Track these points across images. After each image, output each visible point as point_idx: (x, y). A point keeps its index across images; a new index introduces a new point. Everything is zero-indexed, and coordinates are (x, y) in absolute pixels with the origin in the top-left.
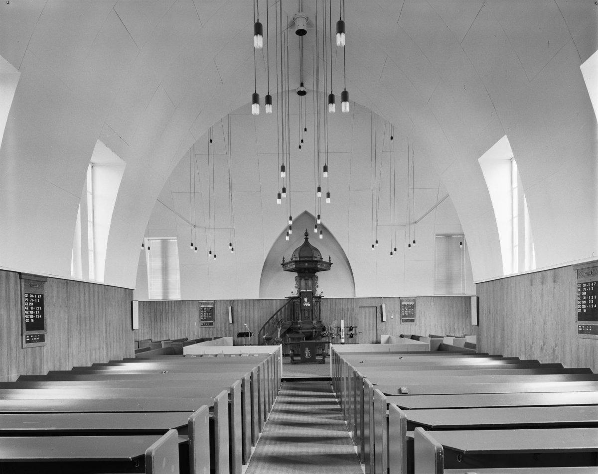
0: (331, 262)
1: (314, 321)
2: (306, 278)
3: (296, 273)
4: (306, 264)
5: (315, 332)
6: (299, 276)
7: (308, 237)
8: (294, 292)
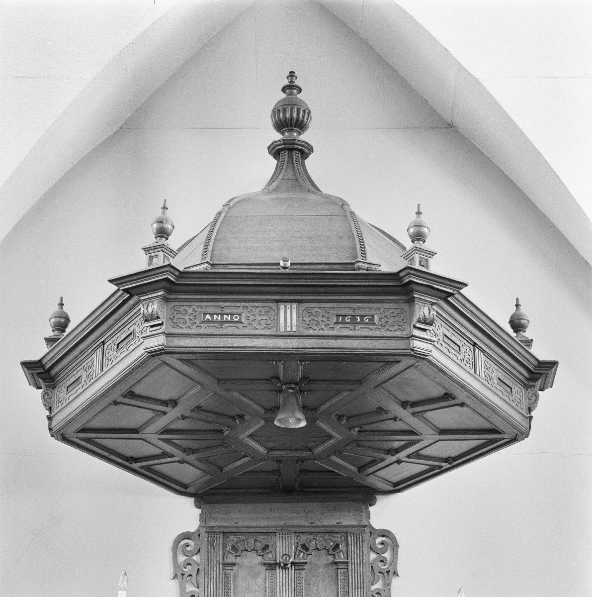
0: (541, 352)
2: (283, 547)
3: (190, 501)
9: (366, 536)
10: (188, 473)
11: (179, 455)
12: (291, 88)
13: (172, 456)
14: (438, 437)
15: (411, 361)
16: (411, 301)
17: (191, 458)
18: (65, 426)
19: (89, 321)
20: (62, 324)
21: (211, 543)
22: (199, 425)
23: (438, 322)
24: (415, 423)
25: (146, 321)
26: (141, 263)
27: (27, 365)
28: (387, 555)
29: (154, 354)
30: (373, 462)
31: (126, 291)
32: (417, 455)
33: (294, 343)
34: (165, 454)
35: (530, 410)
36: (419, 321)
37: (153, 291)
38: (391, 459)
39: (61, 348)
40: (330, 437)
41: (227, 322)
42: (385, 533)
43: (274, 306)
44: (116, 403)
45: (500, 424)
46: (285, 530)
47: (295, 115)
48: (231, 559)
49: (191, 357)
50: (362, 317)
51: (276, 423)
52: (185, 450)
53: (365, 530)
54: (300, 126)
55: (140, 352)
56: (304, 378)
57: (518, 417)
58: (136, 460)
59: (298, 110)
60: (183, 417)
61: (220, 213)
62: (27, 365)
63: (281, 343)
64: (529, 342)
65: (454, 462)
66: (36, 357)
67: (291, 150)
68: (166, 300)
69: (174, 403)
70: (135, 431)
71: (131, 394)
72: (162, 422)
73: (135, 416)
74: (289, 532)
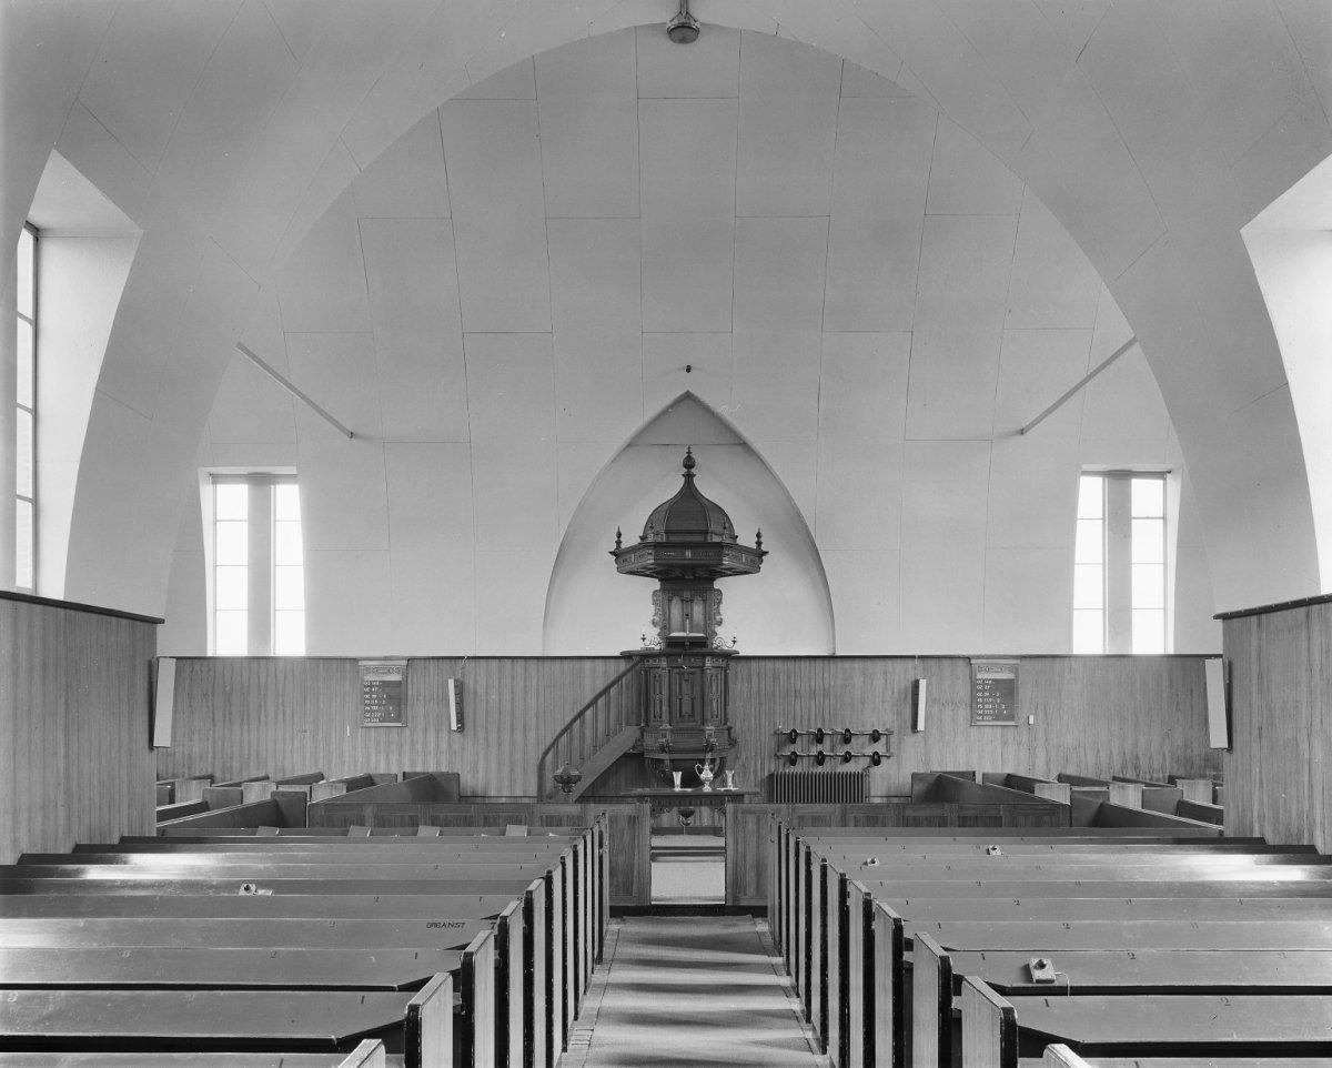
1: (710, 728)
2: (687, 595)
4: (688, 554)
6: (663, 589)
8: (648, 637)
12: (689, 453)
42: (719, 590)
53: (712, 589)
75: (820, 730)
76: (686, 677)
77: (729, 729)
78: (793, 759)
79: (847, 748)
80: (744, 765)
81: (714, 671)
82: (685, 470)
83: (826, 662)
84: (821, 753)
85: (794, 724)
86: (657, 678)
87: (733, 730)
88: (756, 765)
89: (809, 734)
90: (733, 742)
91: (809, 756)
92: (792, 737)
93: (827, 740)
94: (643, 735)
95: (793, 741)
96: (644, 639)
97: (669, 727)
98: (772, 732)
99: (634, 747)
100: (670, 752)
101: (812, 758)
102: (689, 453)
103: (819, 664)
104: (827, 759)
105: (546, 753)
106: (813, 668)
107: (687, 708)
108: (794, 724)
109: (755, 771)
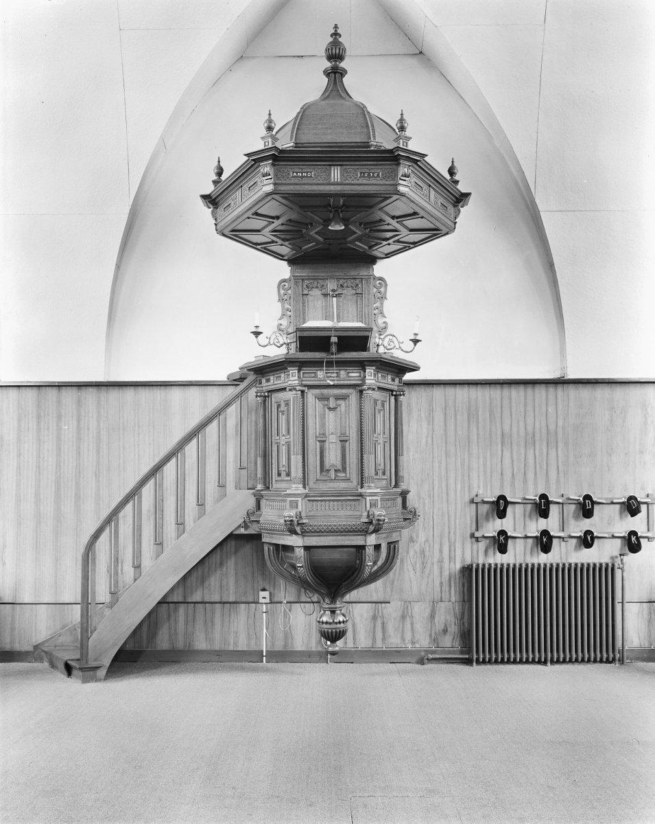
0: (462, 188)
1: (373, 489)
2: (331, 285)
3: (285, 263)
4: (336, 174)
5: (377, 547)
6: (295, 279)
7: (343, 65)
9: (372, 280)
10: (285, 250)
11: (280, 242)
12: (336, 35)
13: (277, 242)
14: (409, 233)
15: (398, 197)
16: (399, 164)
17: (286, 243)
18: (447, 495)
19: (235, 174)
20: (220, 172)
21: (296, 283)
22: (290, 228)
23: (412, 175)
24: (398, 226)
25: (264, 176)
26: (260, 146)
27: (204, 197)
28: (382, 290)
29: (268, 194)
30: (377, 244)
31: (253, 160)
32: (398, 241)
33: (339, 188)
34: (273, 242)
35: (456, 218)
36: (402, 176)
37: (266, 160)
38: (385, 243)
39: (221, 187)
40: (356, 233)
41: (305, 177)
42: (381, 279)
43: (328, 168)
44: (249, 218)
45: (441, 227)
46: (331, 277)
47: (338, 51)
48: (306, 292)
49: (288, 197)
50: (373, 173)
51: (330, 228)
52: (283, 240)
54: (340, 57)
55: (260, 193)
56: (344, 205)
57: (450, 223)
58: (259, 244)
59: (340, 49)
60: (282, 224)
61: (299, 113)
62: (204, 197)
63: (332, 188)
64: (457, 182)
65: (415, 244)
66: (207, 193)
67: (335, 73)
68: (273, 165)
69: (278, 218)
70: (259, 231)
71: (256, 214)
72: (271, 227)
73: (258, 223)
74: (334, 278)
75: (543, 496)
76: (332, 403)
77: (404, 495)
78: (501, 542)
79: (586, 524)
80: (423, 552)
81: (377, 395)
82: (328, 64)
83: (551, 389)
84: (545, 533)
85: (502, 486)
86: (283, 408)
87: (410, 497)
88: (441, 551)
89: (525, 502)
90: (409, 516)
91: (526, 537)
92: (500, 507)
93: (554, 510)
94: (258, 507)
95: (502, 514)
96: (257, 334)
97: (301, 490)
98: (467, 499)
99: (246, 526)
100: (304, 533)
101: (530, 541)
102: (336, 35)
103: (540, 391)
104: (555, 541)
105: (96, 536)
106: (530, 398)
107: (333, 458)
108: (502, 486)
109: (441, 561)
